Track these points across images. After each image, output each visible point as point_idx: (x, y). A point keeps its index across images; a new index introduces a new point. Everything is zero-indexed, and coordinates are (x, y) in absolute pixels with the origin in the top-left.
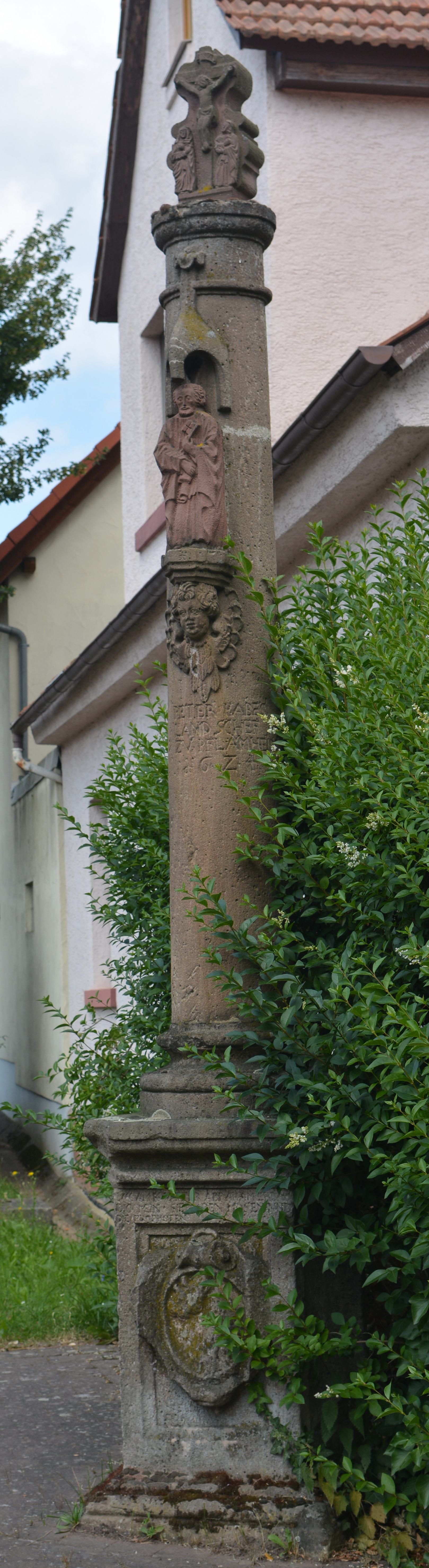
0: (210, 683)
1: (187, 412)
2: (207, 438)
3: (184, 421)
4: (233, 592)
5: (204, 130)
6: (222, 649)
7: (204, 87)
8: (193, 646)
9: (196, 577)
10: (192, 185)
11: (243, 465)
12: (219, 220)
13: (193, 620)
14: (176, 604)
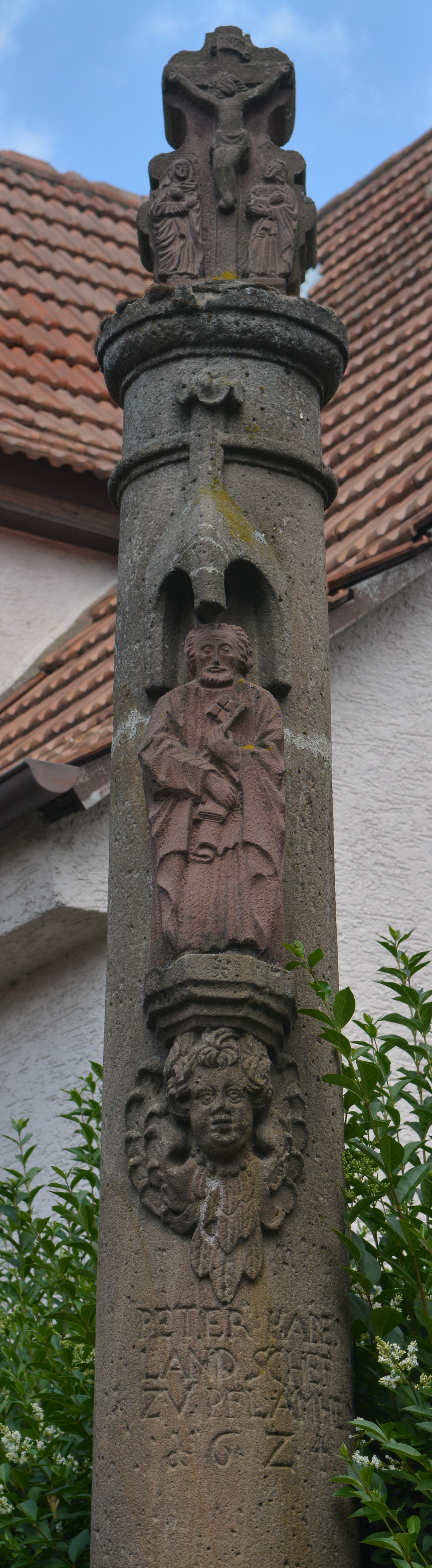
0: (241, 1261)
1: (221, 677)
2: (264, 735)
3: (211, 696)
4: (293, 1066)
5: (227, 170)
6: (275, 1186)
7: (230, 95)
8: (213, 1173)
9: (245, 1019)
10: (197, 265)
11: (304, 806)
12: (276, 326)
13: (229, 1112)
14: (189, 1075)
